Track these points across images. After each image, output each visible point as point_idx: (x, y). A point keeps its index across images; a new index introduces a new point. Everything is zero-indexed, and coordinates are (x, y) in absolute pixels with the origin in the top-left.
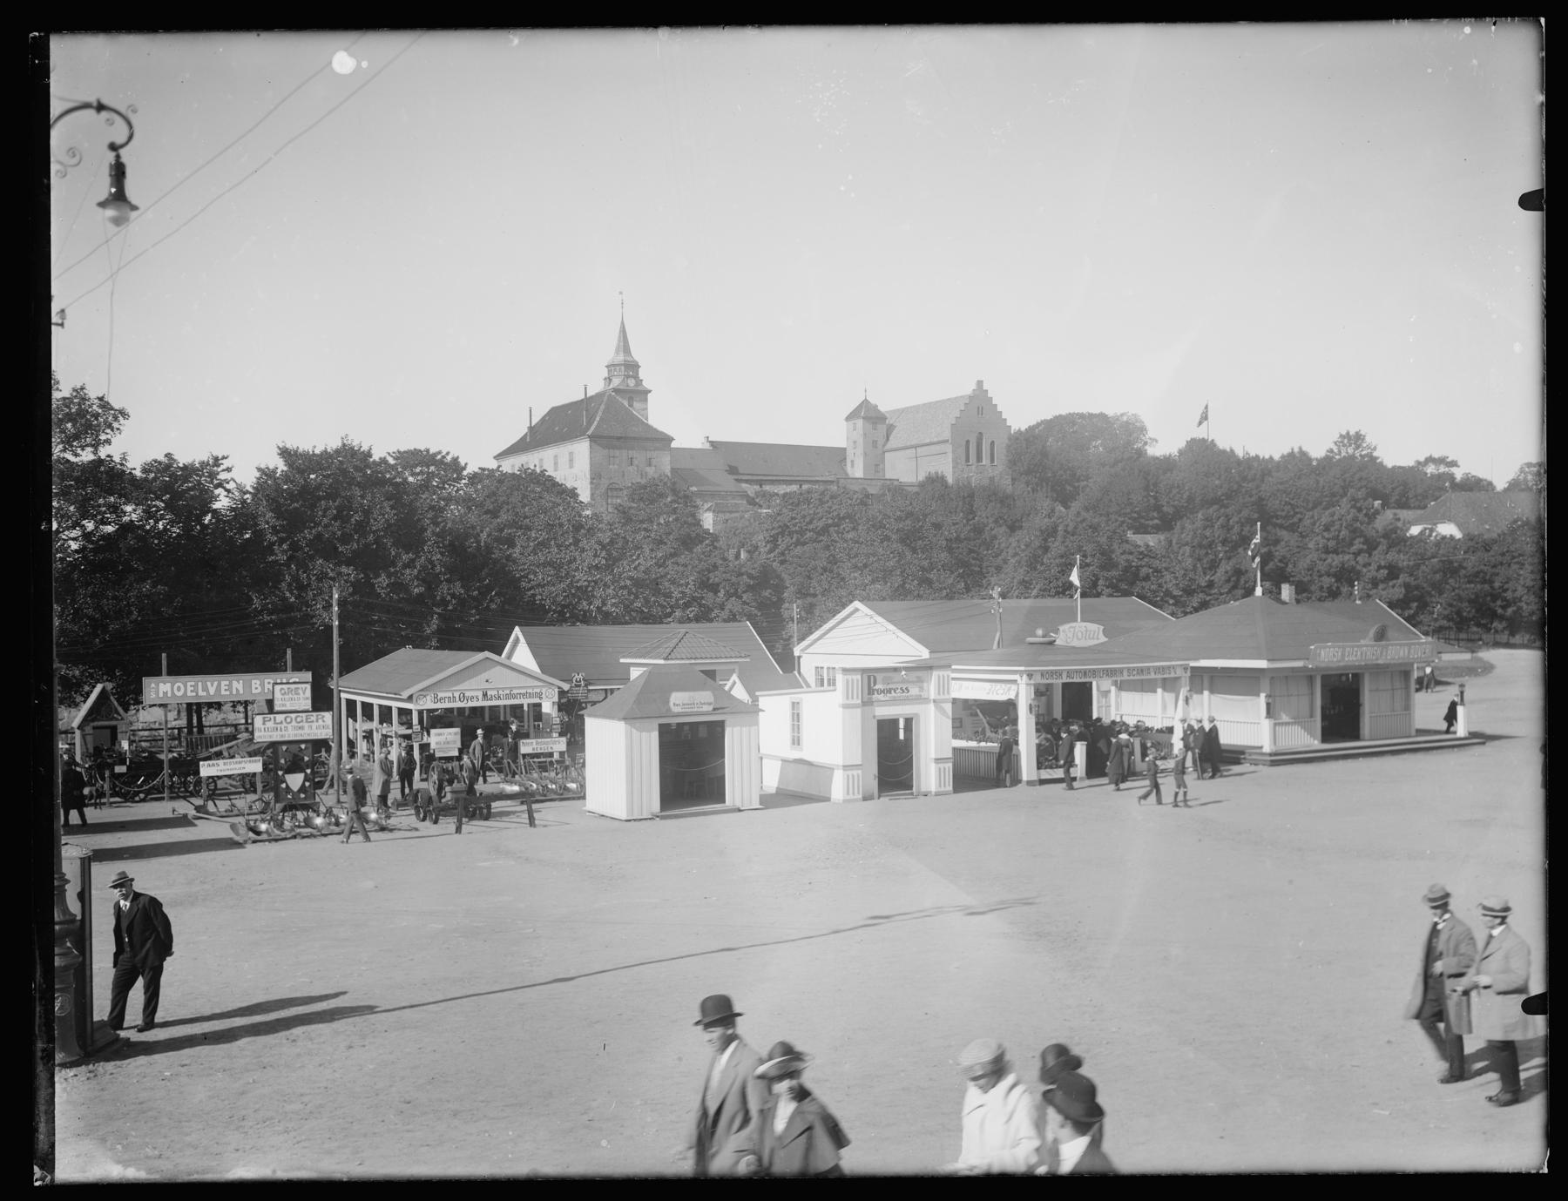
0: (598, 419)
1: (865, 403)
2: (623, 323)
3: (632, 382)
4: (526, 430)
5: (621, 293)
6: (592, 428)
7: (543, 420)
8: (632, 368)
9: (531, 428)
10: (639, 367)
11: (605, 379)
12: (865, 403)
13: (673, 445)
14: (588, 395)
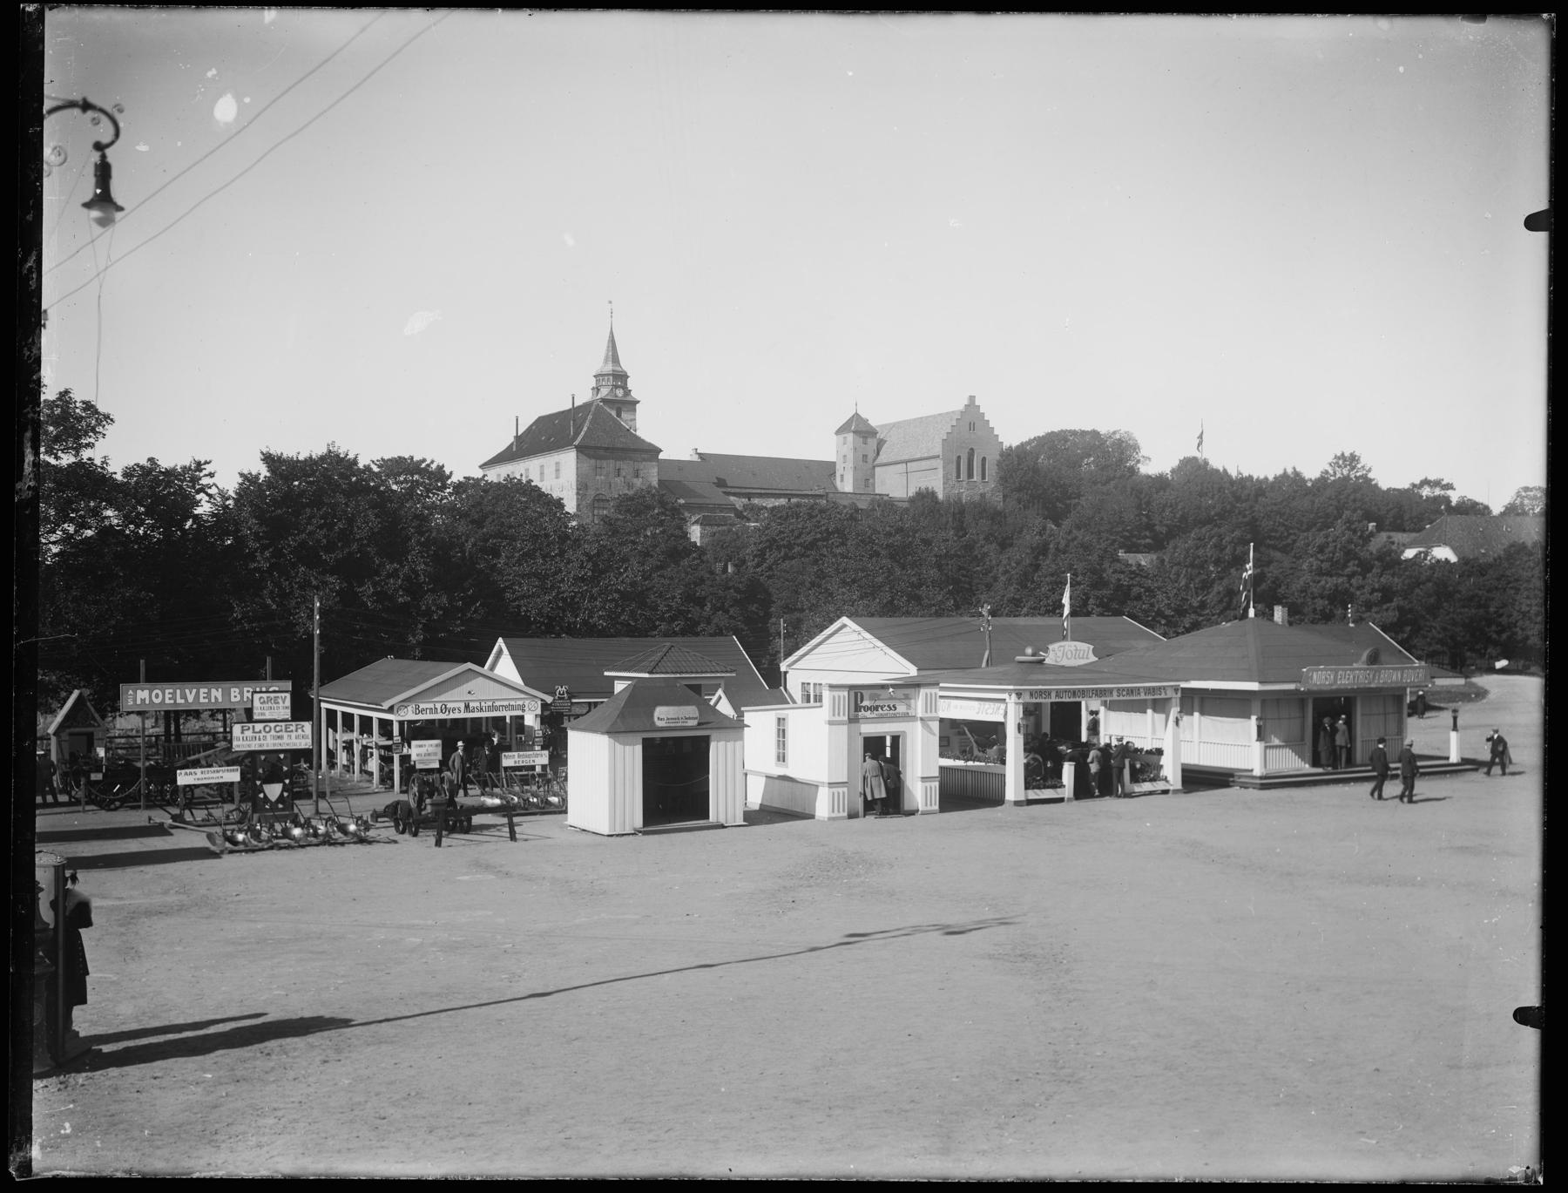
0: (585, 429)
1: (856, 417)
2: (612, 333)
3: (620, 393)
4: (512, 440)
5: (610, 302)
6: (579, 439)
7: (529, 429)
8: (620, 378)
9: (517, 437)
10: (628, 377)
11: (593, 389)
12: (856, 417)
13: (661, 456)
14: (575, 406)
